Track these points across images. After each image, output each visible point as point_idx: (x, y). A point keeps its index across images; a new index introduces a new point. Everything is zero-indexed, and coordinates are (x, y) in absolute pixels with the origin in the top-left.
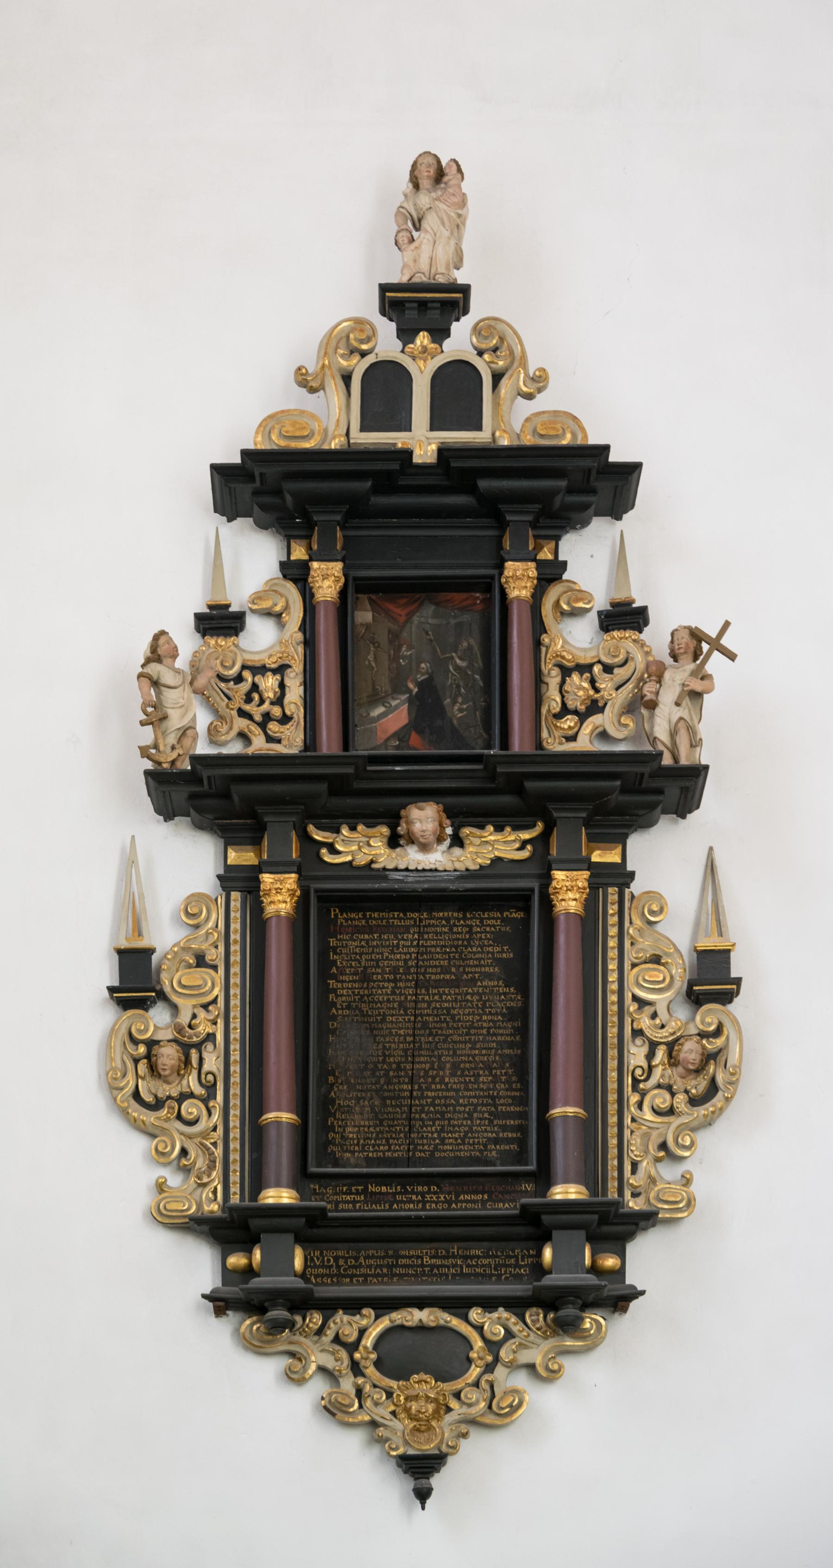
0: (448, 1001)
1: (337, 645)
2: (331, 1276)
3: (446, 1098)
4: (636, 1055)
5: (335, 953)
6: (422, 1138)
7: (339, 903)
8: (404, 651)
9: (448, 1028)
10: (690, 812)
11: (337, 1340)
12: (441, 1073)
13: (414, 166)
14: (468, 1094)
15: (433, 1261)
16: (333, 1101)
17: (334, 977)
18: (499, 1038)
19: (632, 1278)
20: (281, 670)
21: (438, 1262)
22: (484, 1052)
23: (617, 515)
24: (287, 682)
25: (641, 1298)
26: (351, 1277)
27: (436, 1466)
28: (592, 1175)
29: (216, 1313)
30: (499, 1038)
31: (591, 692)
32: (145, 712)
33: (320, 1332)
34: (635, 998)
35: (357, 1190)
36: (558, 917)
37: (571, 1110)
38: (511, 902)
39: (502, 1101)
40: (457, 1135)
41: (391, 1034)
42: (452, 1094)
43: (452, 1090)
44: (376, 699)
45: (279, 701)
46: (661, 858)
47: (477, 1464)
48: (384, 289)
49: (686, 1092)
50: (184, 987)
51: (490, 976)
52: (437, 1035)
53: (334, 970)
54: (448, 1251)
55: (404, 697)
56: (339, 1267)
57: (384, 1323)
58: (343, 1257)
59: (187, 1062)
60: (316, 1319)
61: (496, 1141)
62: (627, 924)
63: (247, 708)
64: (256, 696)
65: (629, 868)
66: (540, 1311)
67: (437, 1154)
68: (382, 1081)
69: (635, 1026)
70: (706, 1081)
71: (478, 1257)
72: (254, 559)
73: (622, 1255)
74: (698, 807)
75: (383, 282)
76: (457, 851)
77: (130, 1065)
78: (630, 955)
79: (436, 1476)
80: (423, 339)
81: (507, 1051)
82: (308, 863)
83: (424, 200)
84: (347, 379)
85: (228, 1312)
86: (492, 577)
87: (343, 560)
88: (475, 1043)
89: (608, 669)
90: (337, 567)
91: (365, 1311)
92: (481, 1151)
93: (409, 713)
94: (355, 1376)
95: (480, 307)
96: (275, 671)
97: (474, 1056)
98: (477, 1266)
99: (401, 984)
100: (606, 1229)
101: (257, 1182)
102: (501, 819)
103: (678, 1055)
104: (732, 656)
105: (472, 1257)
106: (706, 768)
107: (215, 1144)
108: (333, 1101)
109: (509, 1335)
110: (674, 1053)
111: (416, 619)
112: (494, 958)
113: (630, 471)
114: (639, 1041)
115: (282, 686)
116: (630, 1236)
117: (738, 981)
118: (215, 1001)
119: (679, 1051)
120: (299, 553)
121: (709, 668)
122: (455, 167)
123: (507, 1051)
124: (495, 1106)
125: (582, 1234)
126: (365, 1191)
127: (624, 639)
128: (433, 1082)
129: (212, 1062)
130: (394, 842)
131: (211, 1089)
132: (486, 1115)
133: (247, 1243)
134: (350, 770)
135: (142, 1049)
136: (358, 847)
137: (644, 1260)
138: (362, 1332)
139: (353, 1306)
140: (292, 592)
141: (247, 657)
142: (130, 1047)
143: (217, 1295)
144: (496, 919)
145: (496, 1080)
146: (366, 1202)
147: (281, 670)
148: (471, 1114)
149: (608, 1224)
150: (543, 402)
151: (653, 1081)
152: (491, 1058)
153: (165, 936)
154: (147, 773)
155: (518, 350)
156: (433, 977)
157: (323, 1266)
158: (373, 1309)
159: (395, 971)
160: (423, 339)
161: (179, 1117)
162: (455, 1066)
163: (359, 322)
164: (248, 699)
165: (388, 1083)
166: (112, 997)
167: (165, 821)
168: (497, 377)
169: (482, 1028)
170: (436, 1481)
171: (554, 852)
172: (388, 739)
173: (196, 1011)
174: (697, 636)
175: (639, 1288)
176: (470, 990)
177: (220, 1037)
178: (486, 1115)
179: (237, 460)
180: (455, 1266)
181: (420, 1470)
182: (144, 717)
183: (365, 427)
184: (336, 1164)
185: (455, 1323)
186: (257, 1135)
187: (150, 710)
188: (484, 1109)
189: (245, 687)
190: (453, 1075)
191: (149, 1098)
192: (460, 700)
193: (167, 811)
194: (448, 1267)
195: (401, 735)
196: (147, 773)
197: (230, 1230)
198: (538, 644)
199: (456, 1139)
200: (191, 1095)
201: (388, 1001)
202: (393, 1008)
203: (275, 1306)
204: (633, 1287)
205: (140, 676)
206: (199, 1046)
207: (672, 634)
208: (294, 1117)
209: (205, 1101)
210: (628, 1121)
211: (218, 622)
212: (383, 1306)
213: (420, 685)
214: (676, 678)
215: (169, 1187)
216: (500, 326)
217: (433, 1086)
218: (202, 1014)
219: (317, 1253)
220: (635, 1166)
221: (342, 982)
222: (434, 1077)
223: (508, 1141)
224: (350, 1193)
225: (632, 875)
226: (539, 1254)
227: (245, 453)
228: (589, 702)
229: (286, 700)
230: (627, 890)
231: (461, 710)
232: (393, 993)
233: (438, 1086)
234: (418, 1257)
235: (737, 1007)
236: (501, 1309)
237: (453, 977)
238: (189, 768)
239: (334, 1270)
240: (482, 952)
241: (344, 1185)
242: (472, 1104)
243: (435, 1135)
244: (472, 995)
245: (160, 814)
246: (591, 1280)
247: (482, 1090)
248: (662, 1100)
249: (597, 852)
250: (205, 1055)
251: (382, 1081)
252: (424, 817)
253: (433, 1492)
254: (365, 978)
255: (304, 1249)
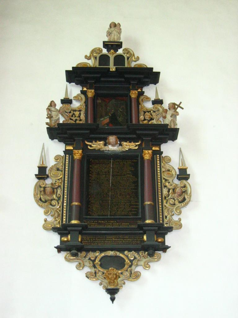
0: (119, 179)
1: (94, 106)
2: (89, 243)
3: (118, 201)
4: (165, 191)
5: (91, 168)
6: (112, 210)
7: (91, 160)
8: (108, 108)
9: (118, 185)
10: (175, 140)
11: (90, 259)
12: (117, 195)
13: (110, 24)
14: (124, 200)
15: (115, 239)
16: (90, 201)
17: (91, 174)
18: (131, 188)
19: (167, 243)
20: (80, 111)
21: (117, 240)
22: (128, 191)
23: (155, 84)
24: (81, 113)
25: (170, 248)
26: (94, 243)
27: (116, 291)
28: (155, 217)
29: (58, 252)
30: (131, 188)
31: (151, 116)
32: (47, 116)
33: (85, 257)
34: (164, 179)
35: (96, 222)
36: (145, 161)
37: (149, 203)
38: (132, 160)
39: (132, 202)
40: (121, 209)
41: (104, 186)
42: (120, 200)
43: (120, 199)
44: (102, 117)
45: (79, 117)
46: (169, 149)
47: (129, 290)
48: (104, 42)
49: (178, 200)
50: (54, 175)
51: (129, 174)
52: (116, 187)
53: (91, 172)
54: (119, 237)
55: (108, 117)
56: (91, 241)
57: (103, 255)
58: (92, 238)
59: (54, 192)
60: (84, 253)
61: (131, 211)
62: (161, 163)
63: (72, 118)
64: (74, 116)
65: (162, 151)
66: (143, 252)
67: (116, 214)
68: (102, 197)
69: (165, 185)
70: (183, 197)
71: (127, 238)
72: (75, 90)
73: (164, 238)
74: (177, 139)
75: (104, 41)
76: (120, 147)
77: (39, 192)
78: (163, 170)
79: (116, 295)
80: (112, 51)
81: (133, 190)
82: (85, 148)
83: (112, 29)
84: (96, 58)
85: (61, 252)
86: (128, 94)
87: (94, 89)
88: (125, 188)
89: (154, 112)
90: (93, 91)
91: (97, 251)
92: (127, 213)
93: (109, 120)
94: (95, 268)
95: (124, 46)
96: (78, 111)
97: (125, 191)
98: (127, 240)
99: (107, 175)
100: (160, 232)
101: (70, 219)
102: (130, 140)
103: (175, 191)
104: (183, 109)
105: (125, 239)
106: (179, 129)
107: (60, 211)
108: (90, 201)
109: (135, 258)
110: (175, 191)
111: (111, 102)
112: (130, 170)
113: (158, 74)
114: (165, 188)
115: (80, 114)
116: (166, 234)
117: (189, 175)
118: (61, 178)
119: (176, 190)
120: (85, 89)
121: (177, 110)
122: (119, 24)
123: (133, 190)
124: (131, 203)
125: (154, 232)
126: (98, 222)
127: (158, 106)
128: (115, 197)
129: (59, 191)
130: (105, 145)
131: (59, 198)
132: (128, 205)
133: (66, 235)
134: (102, 79)
135: (42, 189)
136: (98, 145)
137: (169, 239)
138: (96, 257)
139: (94, 250)
140: (83, 96)
141: (72, 108)
142: (40, 189)
143: (58, 247)
144: (130, 161)
145: (131, 197)
146: (98, 225)
147: (80, 111)
148: (124, 205)
149: (160, 230)
150: (138, 63)
151: (170, 197)
152: (129, 192)
153: (51, 163)
154: (47, 128)
155: (132, 53)
156: (115, 174)
157: (87, 240)
158: (100, 251)
159: (106, 172)
160: (112, 51)
161: (51, 205)
162: (120, 194)
163: (99, 49)
164: (72, 116)
165: (104, 197)
166: (36, 177)
167: (52, 140)
168: (128, 58)
169: (127, 185)
170: (116, 296)
171: (143, 146)
172: (104, 125)
173: (56, 180)
174: (174, 104)
175: (169, 246)
176: (124, 177)
177: (62, 187)
178: (128, 205)
179: (71, 69)
180: (121, 240)
181: (112, 292)
182: (47, 117)
183: (99, 66)
184: (90, 216)
185: (121, 255)
186: (70, 207)
187: (49, 115)
188: (128, 203)
189: (71, 114)
190: (120, 196)
191: (43, 200)
192: (121, 117)
193: (52, 137)
194: (119, 241)
195: (108, 124)
196: (47, 128)
197: (62, 230)
198: (138, 107)
199: (121, 210)
200: (54, 199)
201: (104, 179)
202: (105, 181)
203: (73, 250)
204: (167, 246)
205: (47, 109)
206: (57, 188)
207: (169, 104)
208: (80, 204)
209: (58, 201)
210: (164, 206)
211: (66, 101)
212: (102, 250)
213: (112, 114)
214: (170, 113)
215: (48, 221)
216: (129, 50)
217: (115, 198)
218: (58, 181)
219: (85, 237)
220: (166, 217)
221: (92, 175)
222: (115, 196)
223: (134, 211)
224: (93, 222)
225: (162, 152)
226: (143, 238)
227: (73, 68)
228: (150, 118)
229: (81, 116)
230: (161, 156)
231: (121, 119)
232: (105, 177)
233: (116, 198)
234: (111, 238)
235: (189, 181)
236: (133, 251)
237: (120, 174)
238: (57, 127)
239: (89, 241)
240: (127, 169)
241: (92, 221)
242: (125, 202)
243: (116, 210)
244: (125, 178)
245: (50, 139)
246: (157, 243)
247: (127, 199)
248: (172, 201)
249: (153, 148)
250: (58, 190)
251: (102, 197)
252: (112, 139)
253: (116, 299)
254: (98, 174)
255: (82, 236)
